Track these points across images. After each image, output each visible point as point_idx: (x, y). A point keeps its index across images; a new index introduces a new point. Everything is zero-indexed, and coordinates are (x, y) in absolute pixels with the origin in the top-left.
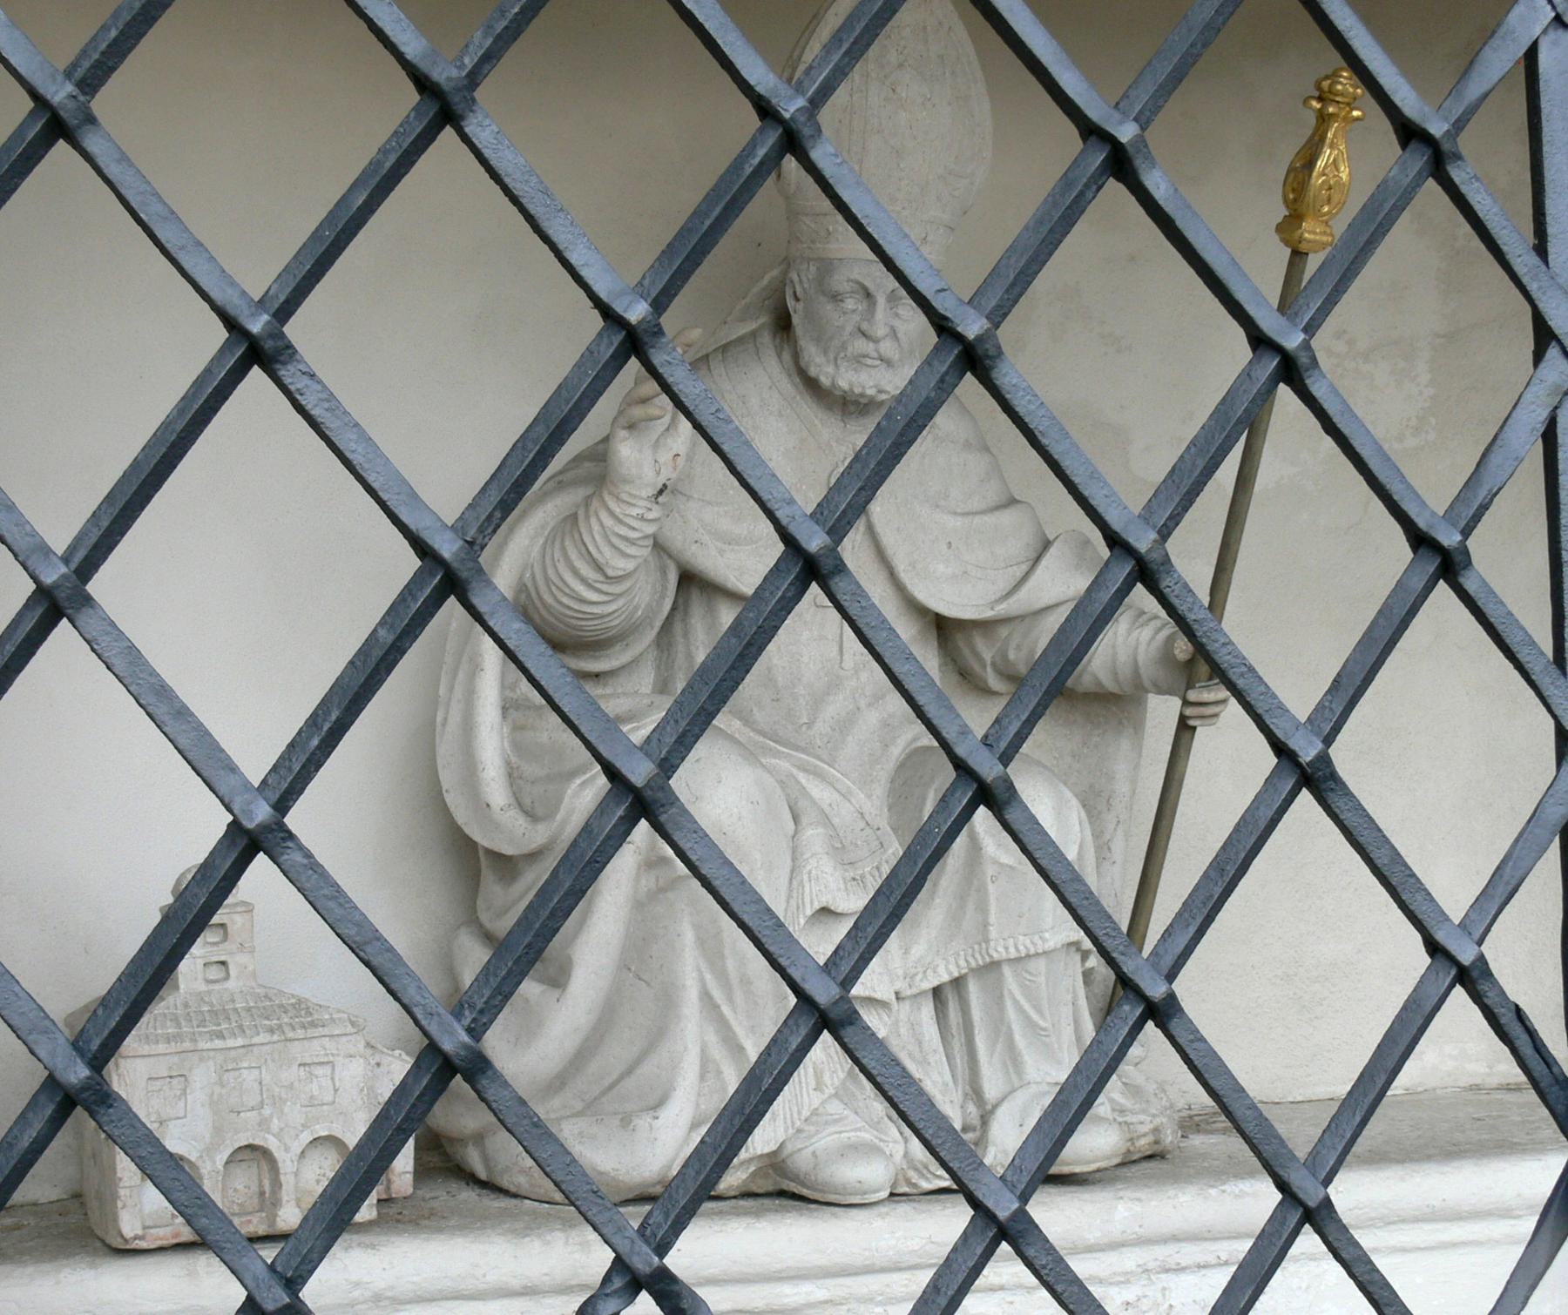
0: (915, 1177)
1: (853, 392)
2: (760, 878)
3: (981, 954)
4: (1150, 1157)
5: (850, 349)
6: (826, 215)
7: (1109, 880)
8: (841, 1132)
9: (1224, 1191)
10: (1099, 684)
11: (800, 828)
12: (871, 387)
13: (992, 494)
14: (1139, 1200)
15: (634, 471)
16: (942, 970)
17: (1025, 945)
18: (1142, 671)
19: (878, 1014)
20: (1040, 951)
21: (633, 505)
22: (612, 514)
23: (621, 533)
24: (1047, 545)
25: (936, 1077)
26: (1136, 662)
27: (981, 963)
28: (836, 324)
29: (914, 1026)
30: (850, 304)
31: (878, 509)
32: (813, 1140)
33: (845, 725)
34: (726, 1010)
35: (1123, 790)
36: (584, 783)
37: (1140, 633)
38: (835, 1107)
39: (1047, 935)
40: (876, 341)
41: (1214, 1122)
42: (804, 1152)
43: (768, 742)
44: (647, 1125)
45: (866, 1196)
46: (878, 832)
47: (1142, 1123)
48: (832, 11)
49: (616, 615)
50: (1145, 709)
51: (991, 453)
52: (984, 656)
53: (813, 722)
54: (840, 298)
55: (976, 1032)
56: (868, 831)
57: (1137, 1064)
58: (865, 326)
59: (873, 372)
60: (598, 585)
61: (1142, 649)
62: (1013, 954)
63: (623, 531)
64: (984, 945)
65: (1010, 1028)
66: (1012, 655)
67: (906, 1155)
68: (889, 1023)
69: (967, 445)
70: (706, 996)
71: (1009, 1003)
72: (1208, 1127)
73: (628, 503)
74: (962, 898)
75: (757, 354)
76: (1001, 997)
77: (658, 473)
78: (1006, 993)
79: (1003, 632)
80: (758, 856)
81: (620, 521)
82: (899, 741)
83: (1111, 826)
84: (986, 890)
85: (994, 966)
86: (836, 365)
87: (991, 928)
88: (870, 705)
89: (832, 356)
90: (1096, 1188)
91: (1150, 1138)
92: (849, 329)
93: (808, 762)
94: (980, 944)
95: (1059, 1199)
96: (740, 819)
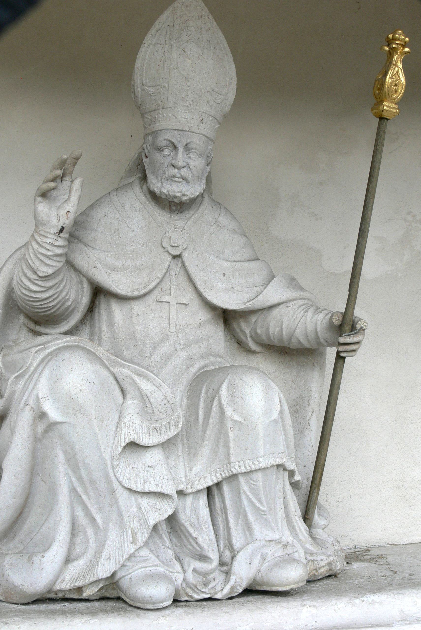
0: (190, 592)
1: (170, 195)
2: (95, 424)
3: (227, 470)
4: (330, 576)
5: (167, 173)
6: (154, 111)
7: (309, 439)
8: (146, 567)
9: (363, 601)
10: (300, 342)
11: (125, 400)
12: (178, 192)
13: (247, 253)
14: (315, 606)
15: (45, 219)
16: (208, 479)
17: (249, 465)
18: (319, 334)
19: (168, 502)
20: (257, 468)
21: (47, 237)
22: (38, 243)
23: (42, 252)
24: (273, 277)
25: (205, 536)
26: (316, 330)
27: (228, 475)
28: (161, 162)
29: (195, 509)
30: (166, 152)
31: (187, 255)
32: (130, 571)
33: (167, 358)
34: (85, 498)
35: (315, 396)
36: (17, 377)
37: (318, 316)
38: (145, 552)
39: (261, 460)
40: (179, 168)
41: (365, 555)
42: (127, 577)
43: (117, 359)
44: (38, 560)
45: (156, 605)
46: (173, 405)
47: (322, 560)
48: (157, 21)
49: (51, 300)
50: (325, 359)
51: (246, 237)
52: (246, 331)
53: (152, 356)
54: (161, 150)
55: (229, 512)
56: (168, 405)
57: (323, 528)
58: (173, 162)
59: (179, 185)
60: (36, 282)
61: (319, 324)
62: (243, 470)
63: (43, 251)
64: (228, 465)
65: (245, 510)
66: (259, 331)
67: (184, 580)
68: (173, 507)
69: (234, 232)
70: (73, 490)
71: (243, 497)
72: (362, 558)
73: (44, 236)
74: (217, 441)
75: (132, 187)
76: (240, 493)
77: (59, 220)
78: (242, 492)
79: (253, 318)
80: (93, 412)
81: (41, 246)
82: (196, 366)
83: (310, 413)
84: (228, 436)
85: (233, 477)
86: (162, 183)
87: (232, 456)
88: (182, 349)
89: (160, 179)
90: (294, 597)
91: (327, 568)
92: (166, 164)
93: (139, 370)
94: (227, 465)
95: (270, 606)
96: (81, 391)
